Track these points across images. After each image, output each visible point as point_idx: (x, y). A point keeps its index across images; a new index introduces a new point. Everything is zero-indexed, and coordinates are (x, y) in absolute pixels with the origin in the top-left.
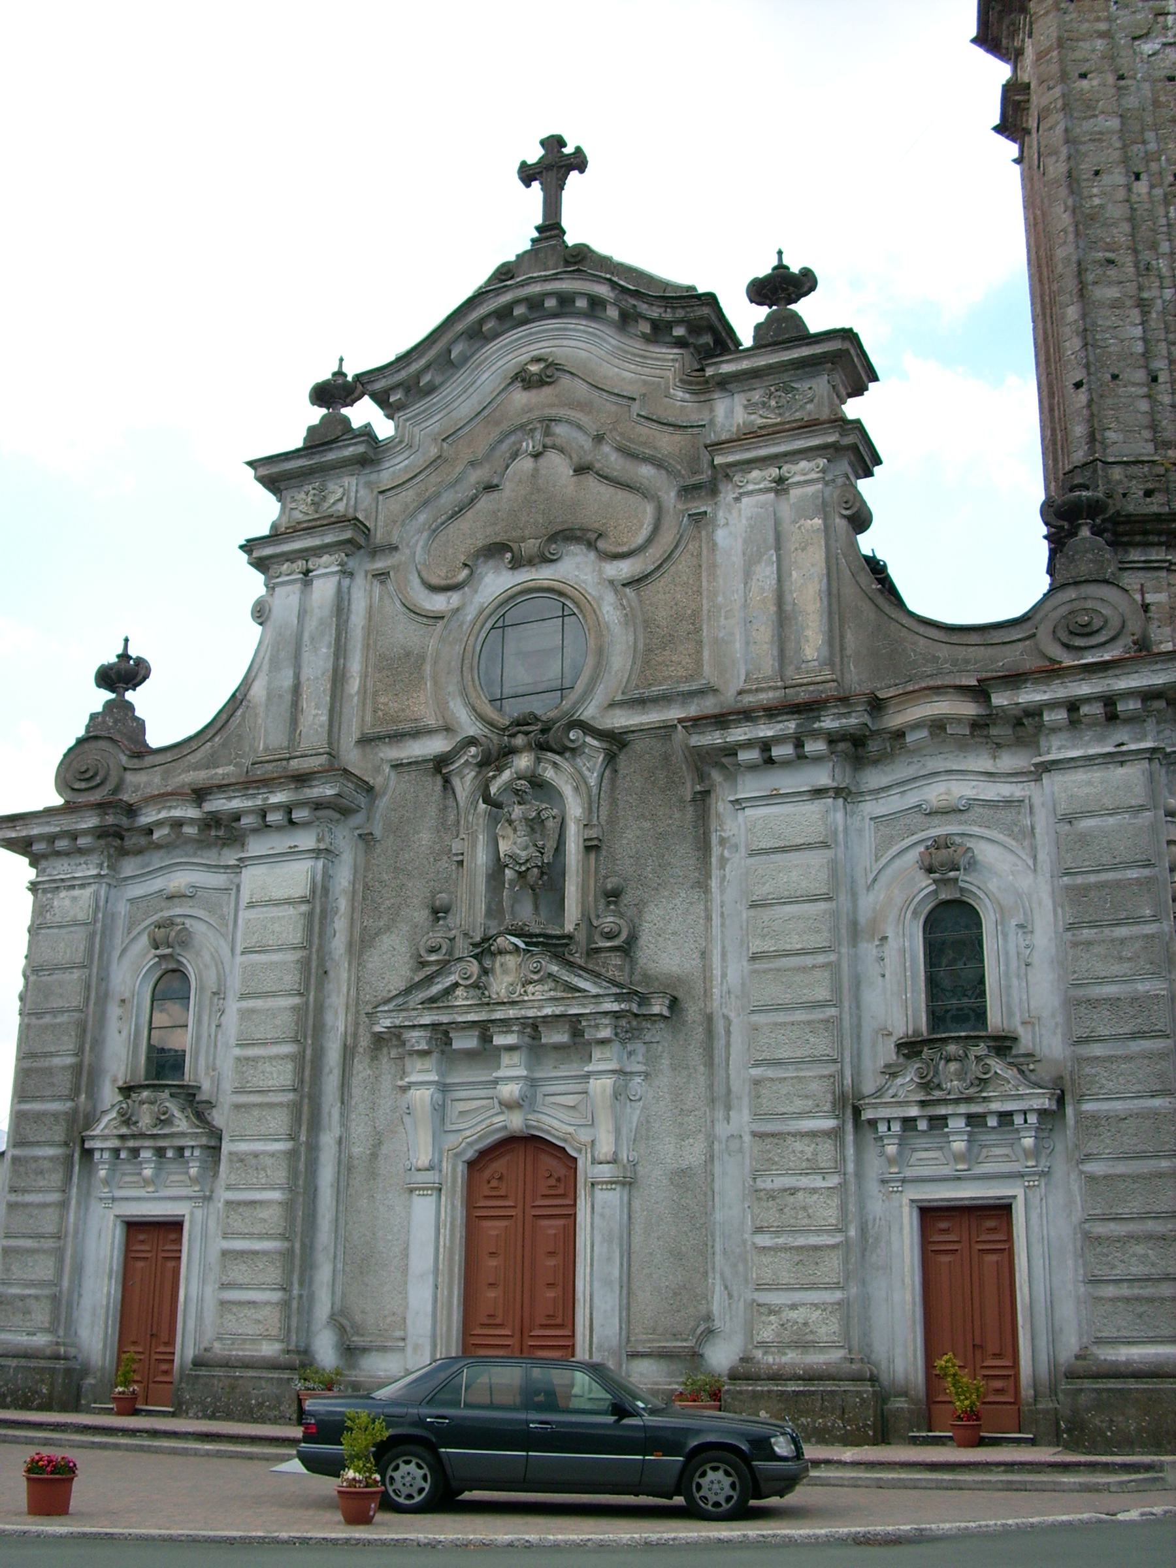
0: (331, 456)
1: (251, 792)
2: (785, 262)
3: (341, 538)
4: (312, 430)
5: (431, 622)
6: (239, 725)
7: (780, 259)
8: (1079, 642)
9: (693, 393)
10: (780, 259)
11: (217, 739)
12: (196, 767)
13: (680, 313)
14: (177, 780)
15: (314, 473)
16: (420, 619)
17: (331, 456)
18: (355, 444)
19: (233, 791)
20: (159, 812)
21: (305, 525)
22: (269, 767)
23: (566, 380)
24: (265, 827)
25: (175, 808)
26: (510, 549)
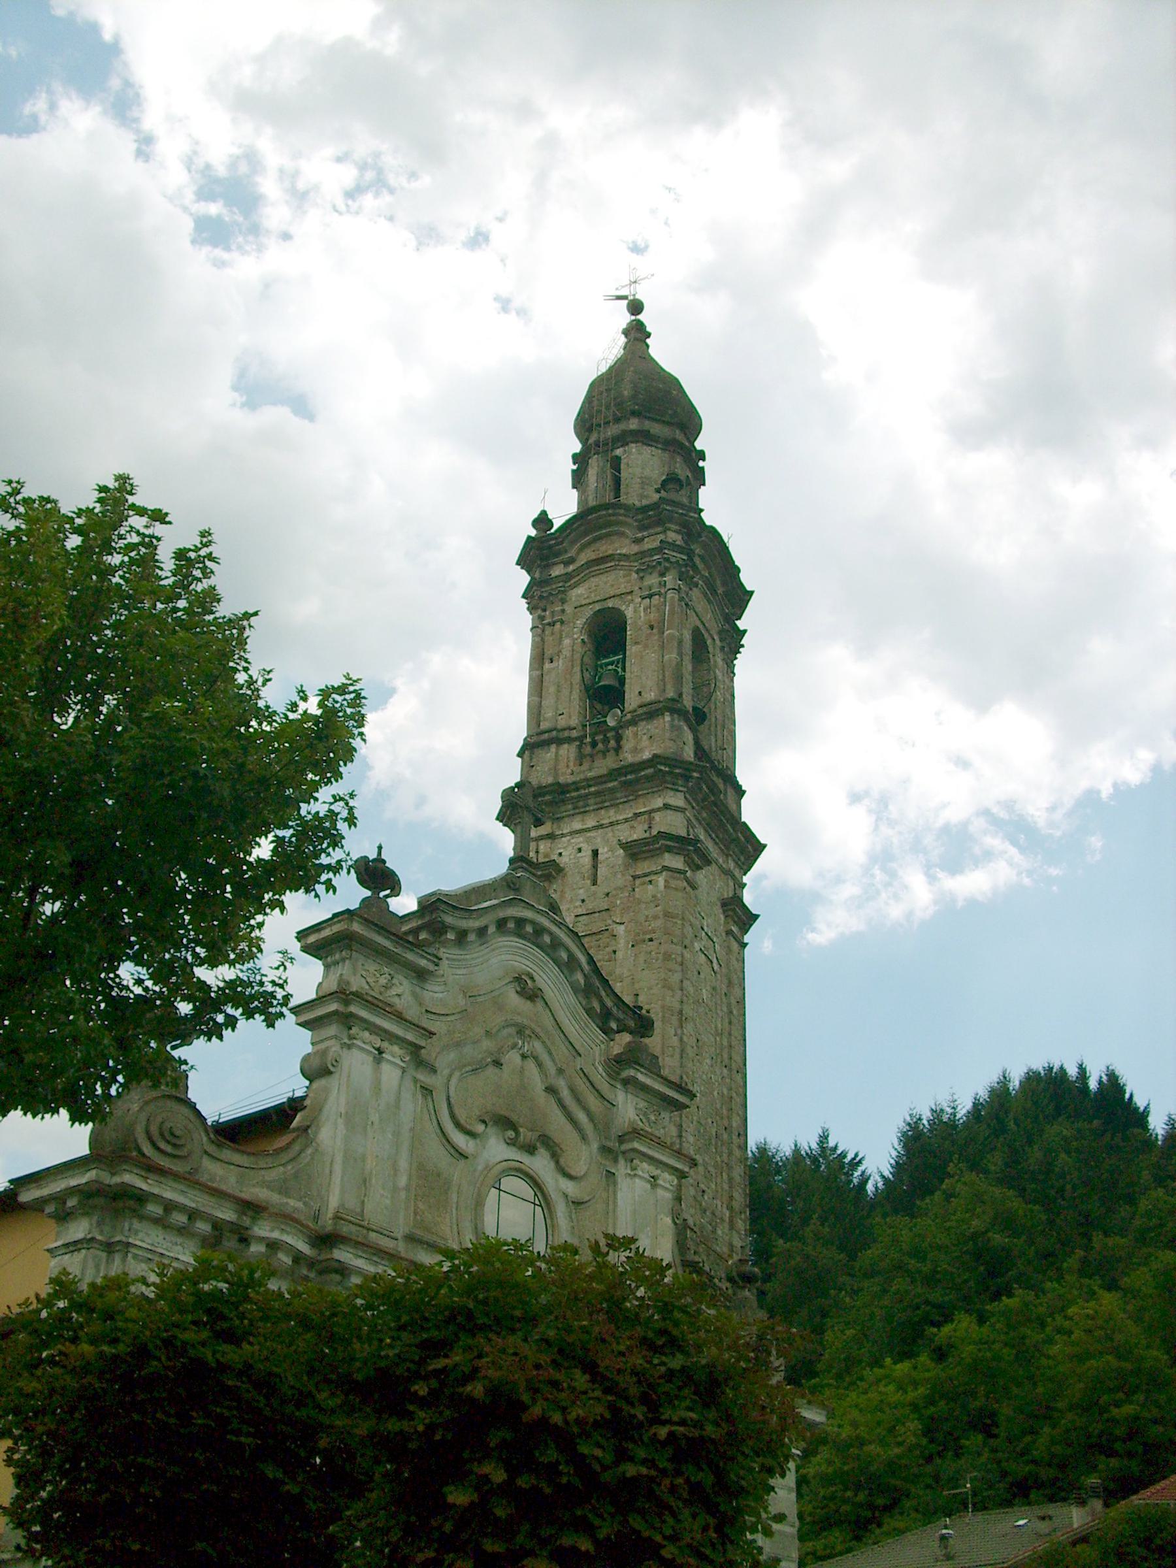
0: (410, 956)
1: (375, 1258)
2: (383, 857)
3: (417, 1042)
4: (364, 900)
5: (456, 1155)
6: (308, 1164)
7: (379, 853)
8: (162, 1145)
9: (609, 1075)
10: (379, 853)
11: (289, 1167)
12: (269, 1186)
13: (621, 1016)
14: (252, 1190)
15: (381, 954)
16: (449, 1147)
17: (410, 956)
18: (429, 960)
19: (364, 1252)
20: (272, 1231)
21: (370, 999)
22: (353, 1228)
23: (540, 1004)
24: (160, 1222)
25: (288, 1233)
26: (516, 1130)
